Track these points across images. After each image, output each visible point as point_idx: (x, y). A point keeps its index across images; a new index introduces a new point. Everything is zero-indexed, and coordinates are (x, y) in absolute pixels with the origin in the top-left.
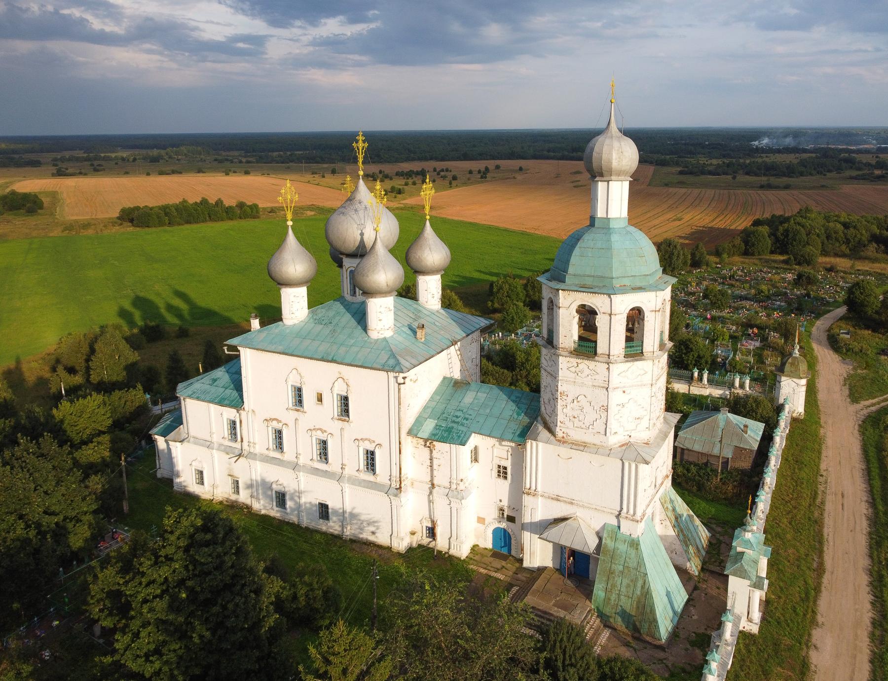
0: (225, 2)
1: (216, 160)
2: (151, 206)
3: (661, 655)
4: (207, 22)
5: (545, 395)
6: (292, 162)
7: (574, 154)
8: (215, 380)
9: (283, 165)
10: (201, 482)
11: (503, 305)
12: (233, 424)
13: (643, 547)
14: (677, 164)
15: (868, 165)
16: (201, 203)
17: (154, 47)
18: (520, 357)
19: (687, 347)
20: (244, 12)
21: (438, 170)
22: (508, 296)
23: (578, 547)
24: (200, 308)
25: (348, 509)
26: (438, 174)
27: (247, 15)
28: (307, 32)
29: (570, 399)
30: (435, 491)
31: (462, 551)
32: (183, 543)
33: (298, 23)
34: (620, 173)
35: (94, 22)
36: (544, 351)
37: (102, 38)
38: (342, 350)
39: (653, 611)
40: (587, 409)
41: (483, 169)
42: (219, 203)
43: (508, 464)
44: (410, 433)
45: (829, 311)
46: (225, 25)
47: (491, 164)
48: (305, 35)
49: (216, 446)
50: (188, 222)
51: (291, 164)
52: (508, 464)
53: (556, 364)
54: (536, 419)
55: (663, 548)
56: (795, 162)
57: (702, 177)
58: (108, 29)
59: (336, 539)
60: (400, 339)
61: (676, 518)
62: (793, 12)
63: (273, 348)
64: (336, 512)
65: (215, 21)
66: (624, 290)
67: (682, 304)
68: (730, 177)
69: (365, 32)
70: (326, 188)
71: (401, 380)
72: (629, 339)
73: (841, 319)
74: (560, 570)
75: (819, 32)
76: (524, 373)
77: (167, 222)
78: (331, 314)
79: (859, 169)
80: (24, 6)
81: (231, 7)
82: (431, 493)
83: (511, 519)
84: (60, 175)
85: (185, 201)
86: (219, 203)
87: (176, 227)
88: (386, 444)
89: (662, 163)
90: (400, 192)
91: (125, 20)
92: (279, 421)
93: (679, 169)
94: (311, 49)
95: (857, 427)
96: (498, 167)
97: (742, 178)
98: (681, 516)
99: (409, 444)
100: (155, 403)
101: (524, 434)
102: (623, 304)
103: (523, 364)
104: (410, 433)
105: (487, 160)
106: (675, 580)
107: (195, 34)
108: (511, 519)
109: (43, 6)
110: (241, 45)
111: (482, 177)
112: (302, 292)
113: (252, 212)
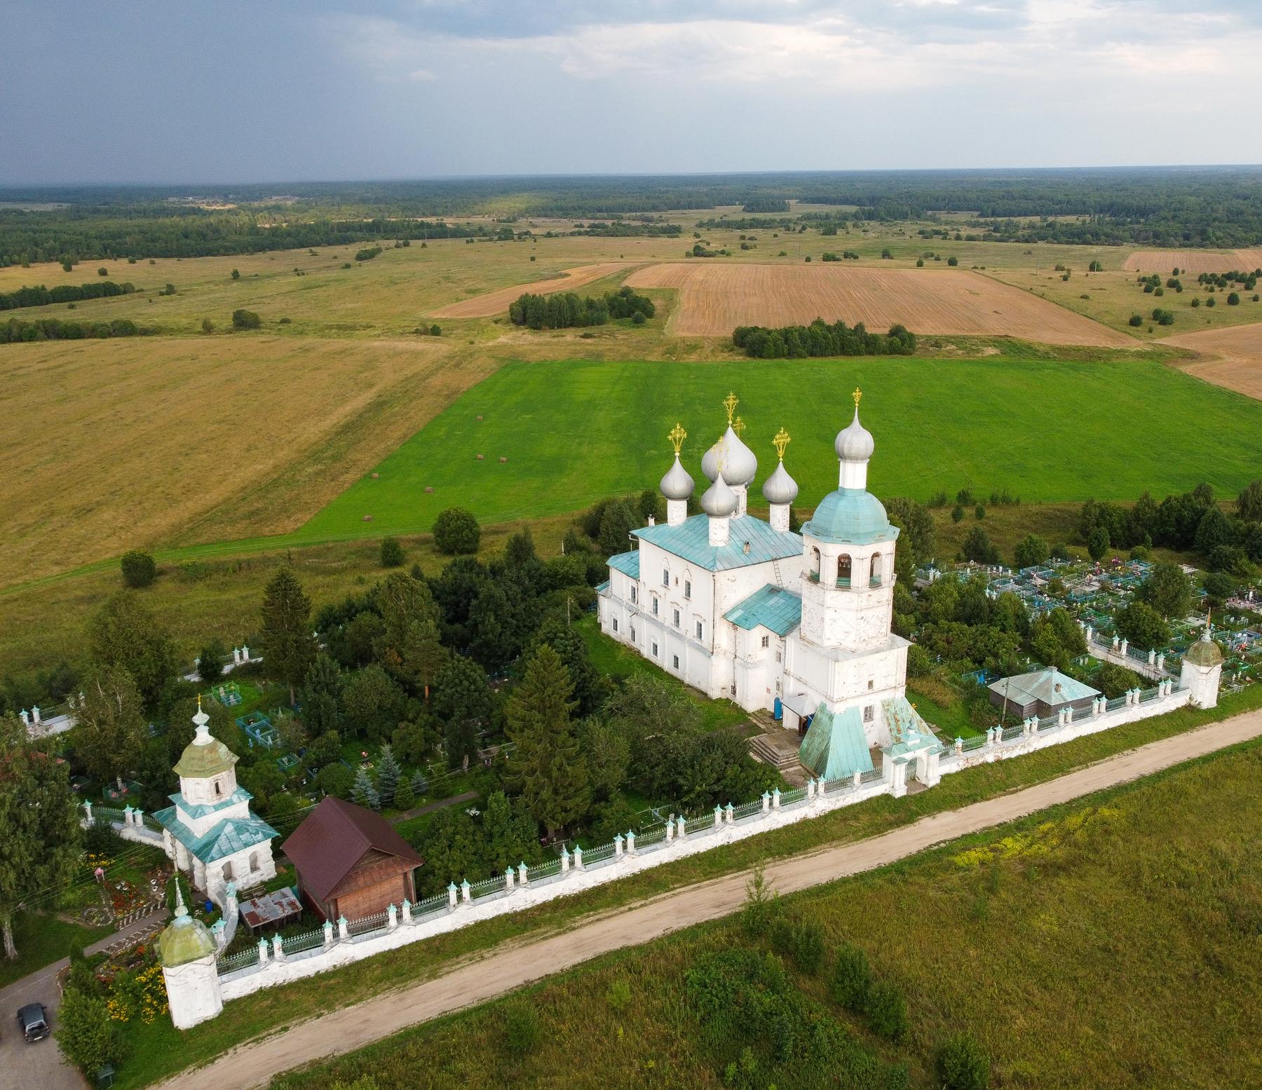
12: (634, 589)
34: (855, 459)
44: (724, 616)
50: (812, 355)
51: (1041, 244)
70: (1052, 305)
85: (819, 322)
87: (796, 361)
104: (724, 616)
112: (683, 505)
113: (903, 345)
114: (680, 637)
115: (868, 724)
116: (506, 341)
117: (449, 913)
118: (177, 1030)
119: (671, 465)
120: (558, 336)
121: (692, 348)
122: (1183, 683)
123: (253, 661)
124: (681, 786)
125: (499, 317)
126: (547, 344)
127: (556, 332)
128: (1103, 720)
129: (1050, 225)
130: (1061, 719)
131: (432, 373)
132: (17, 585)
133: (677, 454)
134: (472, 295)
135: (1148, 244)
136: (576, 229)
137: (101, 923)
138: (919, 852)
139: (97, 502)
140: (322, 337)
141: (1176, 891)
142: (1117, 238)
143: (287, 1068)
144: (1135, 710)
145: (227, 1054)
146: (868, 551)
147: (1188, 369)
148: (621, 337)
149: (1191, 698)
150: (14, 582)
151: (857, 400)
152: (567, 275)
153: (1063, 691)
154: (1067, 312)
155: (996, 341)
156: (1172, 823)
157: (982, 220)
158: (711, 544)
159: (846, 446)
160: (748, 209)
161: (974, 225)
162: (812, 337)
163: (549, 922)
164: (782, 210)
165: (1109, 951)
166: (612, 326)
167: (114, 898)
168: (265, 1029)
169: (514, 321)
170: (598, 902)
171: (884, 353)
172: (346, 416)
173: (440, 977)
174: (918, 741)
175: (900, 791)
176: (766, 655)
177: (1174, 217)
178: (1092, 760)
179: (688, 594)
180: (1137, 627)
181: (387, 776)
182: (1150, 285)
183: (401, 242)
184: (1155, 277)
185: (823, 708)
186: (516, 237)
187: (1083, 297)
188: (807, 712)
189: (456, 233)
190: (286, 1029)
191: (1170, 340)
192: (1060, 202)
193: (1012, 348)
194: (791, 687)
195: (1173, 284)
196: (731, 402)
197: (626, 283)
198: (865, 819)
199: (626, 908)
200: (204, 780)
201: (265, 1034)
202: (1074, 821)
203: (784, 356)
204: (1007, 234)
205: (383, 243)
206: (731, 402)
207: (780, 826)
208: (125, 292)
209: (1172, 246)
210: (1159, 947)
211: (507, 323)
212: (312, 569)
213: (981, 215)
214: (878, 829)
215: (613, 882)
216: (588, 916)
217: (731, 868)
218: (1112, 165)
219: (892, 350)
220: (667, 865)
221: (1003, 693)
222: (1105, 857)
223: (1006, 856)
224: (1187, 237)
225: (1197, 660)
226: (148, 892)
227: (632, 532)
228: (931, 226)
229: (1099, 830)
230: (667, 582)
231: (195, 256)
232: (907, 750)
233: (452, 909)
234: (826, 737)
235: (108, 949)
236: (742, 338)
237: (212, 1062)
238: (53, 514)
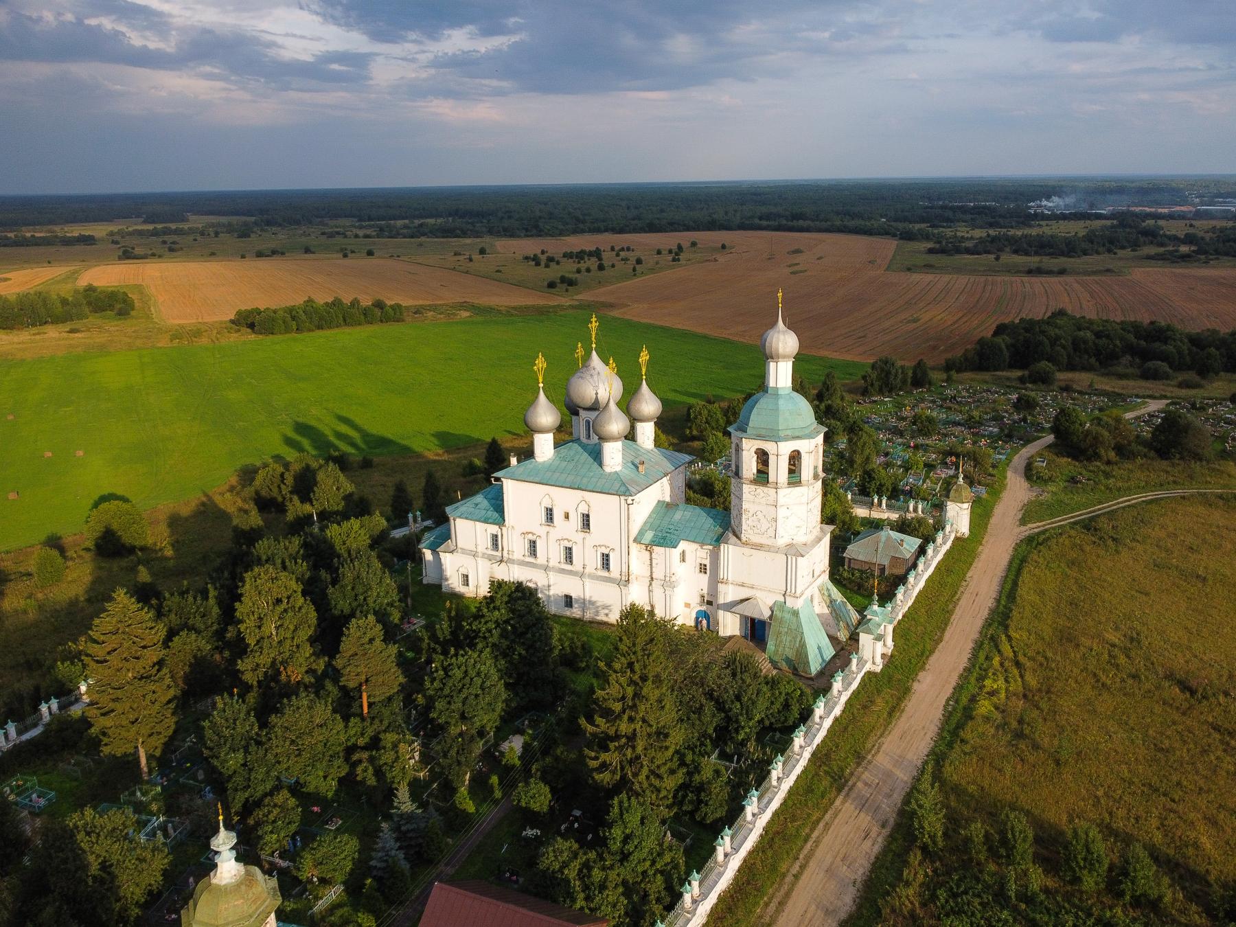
0: (308, 6)
1: (323, 234)
2: (274, 307)
3: (811, 682)
4: (287, 35)
5: (734, 512)
7: (795, 223)
8: (477, 505)
9: (412, 240)
10: (466, 583)
11: (701, 432)
12: (495, 538)
13: (801, 615)
14: (927, 237)
15: (1175, 239)
16: (333, 303)
17: (216, 71)
18: (718, 486)
19: (870, 476)
20: (335, 21)
21: (617, 248)
22: (707, 422)
23: (756, 616)
24: (372, 435)
25: (587, 597)
26: (618, 255)
27: (339, 25)
28: (425, 48)
29: (750, 515)
30: (653, 583)
32: (505, 599)
33: (413, 35)
34: (785, 357)
35: (132, 36)
36: (733, 480)
37: (145, 59)
38: (585, 480)
39: (807, 656)
40: (763, 520)
41: (675, 248)
43: (707, 562)
44: (635, 540)
45: (1040, 438)
46: (311, 39)
47: (685, 238)
48: (424, 52)
49: (480, 555)
50: (320, 327)
51: (423, 239)
52: (707, 562)
53: (741, 489)
54: (727, 529)
55: (819, 624)
56: (1082, 233)
57: (958, 257)
58: (152, 46)
59: (576, 622)
60: (626, 472)
61: (831, 602)
62: (1095, 15)
63: (531, 479)
64: (577, 601)
65: (298, 32)
66: (787, 439)
67: (890, 430)
68: (992, 257)
69: (505, 48)
71: (630, 501)
72: (791, 472)
73: (1049, 446)
74: (745, 637)
75: (1130, 43)
76: (721, 500)
77: (295, 327)
78: (572, 453)
79: (1162, 245)
80: (35, 15)
81: (317, 14)
82: (651, 584)
83: (710, 603)
84: (128, 258)
88: (618, 549)
89: (908, 236)
90: (571, 283)
91: (174, 33)
92: (533, 534)
93: (930, 245)
94: (433, 71)
95: (1013, 545)
96: (694, 244)
97: (1008, 258)
98: (835, 601)
99: (634, 548)
101: (719, 540)
102: (786, 448)
103: (720, 492)
104: (635, 540)
105: (680, 231)
106: (826, 642)
107: (272, 52)
108: (710, 603)
109: (59, 14)
110: (335, 67)
111: (674, 260)
112: (549, 438)
120: (39, 334)
121: (197, 333)
123: (26, 736)
129: (421, 225)
133: (541, 385)
135: (501, 236)
152: (10, 279)
161: (361, 227)
164: (183, 221)
166: (93, 320)
182: (536, 260)
206: (594, 324)
209: (519, 237)
213: (360, 220)
219: (385, 319)
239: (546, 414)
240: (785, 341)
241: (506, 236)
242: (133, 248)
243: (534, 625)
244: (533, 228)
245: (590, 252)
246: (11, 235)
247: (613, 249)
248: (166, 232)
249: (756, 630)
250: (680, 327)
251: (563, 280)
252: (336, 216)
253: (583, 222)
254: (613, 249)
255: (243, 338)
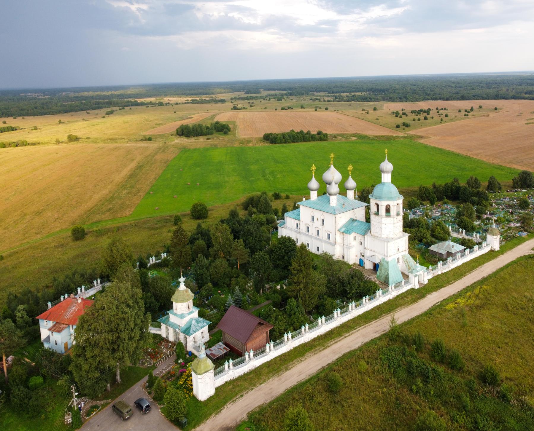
1: (311, 99)
6: (353, 100)
13: (389, 264)
17: (276, 31)
31: (351, 263)
33: (357, 11)
42: (309, 132)
44: (338, 230)
48: (362, 18)
50: (293, 142)
51: (353, 102)
60: (337, 206)
80: (211, 14)
85: (293, 131)
86: (309, 132)
100: (278, 220)
104: (338, 230)
110: (323, 26)
114: (320, 240)
115: (398, 264)
116: (178, 142)
117: (285, 345)
118: (200, 402)
119: (349, 177)
120: (197, 139)
121: (249, 141)
122: (488, 243)
123: (157, 262)
124: (347, 291)
125: (172, 133)
126: (194, 142)
127: (196, 138)
128: (469, 257)
129: (354, 96)
130: (458, 257)
131: (156, 153)
132: (25, 243)
133: (313, 175)
134: (157, 126)
135: (388, 101)
136: (187, 101)
137: (149, 365)
138: (432, 307)
139: (43, 209)
140: (105, 143)
141: (521, 311)
142: (377, 99)
143: (250, 410)
144: (477, 253)
145: (224, 408)
146: (395, 203)
147: (422, 141)
148: (221, 139)
149: (492, 248)
150: (23, 242)
151: (386, 153)
152: (192, 118)
153: (455, 247)
154: (374, 124)
155: (355, 135)
156: (507, 289)
157: (330, 95)
158: (331, 205)
159: (385, 168)
160: (247, 93)
161: (328, 96)
162: (293, 136)
163: (319, 345)
164: (259, 93)
165: (512, 333)
166: (216, 135)
167: (149, 355)
168: (234, 396)
169: (178, 135)
170: (333, 336)
171: (318, 140)
172: (129, 172)
173: (290, 369)
174: (420, 268)
175: (417, 287)
176: (355, 244)
177: (394, 92)
178: (471, 270)
179: (323, 223)
180: (465, 225)
181: (238, 298)
182: (397, 114)
183: (121, 108)
184: (397, 112)
185: (383, 259)
186: (165, 105)
187: (376, 119)
188: (377, 262)
189: (142, 104)
190: (242, 396)
191: (411, 132)
192: (354, 88)
193: (362, 138)
194: (368, 254)
195: (404, 114)
196: (332, 156)
197: (216, 120)
198: (409, 297)
199: (343, 337)
200: (184, 303)
201: (235, 399)
202: (477, 291)
203: (283, 143)
204: (341, 99)
205: (114, 108)
206: (332, 156)
207: (382, 302)
208: (16, 130)
209: (396, 101)
210: (526, 330)
211: (176, 135)
212: (148, 228)
213: (329, 93)
214: (415, 301)
215: (334, 328)
216: (332, 341)
217: (373, 319)
218: (399, 74)
219: (321, 139)
220: (350, 320)
221: (436, 250)
222: (493, 302)
223: (461, 305)
224: (400, 98)
225: (492, 234)
226: (162, 351)
227: (297, 203)
228: (314, 98)
229: (486, 294)
230: (313, 220)
231: (40, 115)
232: (418, 272)
233: (286, 343)
234: (387, 270)
235: (157, 374)
236: (267, 137)
237: (220, 411)
238: (25, 215)
239: (314, 184)
240: (387, 166)
241: (390, 101)
242: (238, 105)
243: (292, 251)
244: (403, 97)
245: (425, 110)
246: (198, 99)
247: (437, 109)
248: (252, 98)
249: (376, 267)
250: (449, 149)
251: (404, 124)
252: (320, 91)
253: (429, 95)
254: (437, 109)
255: (264, 145)
